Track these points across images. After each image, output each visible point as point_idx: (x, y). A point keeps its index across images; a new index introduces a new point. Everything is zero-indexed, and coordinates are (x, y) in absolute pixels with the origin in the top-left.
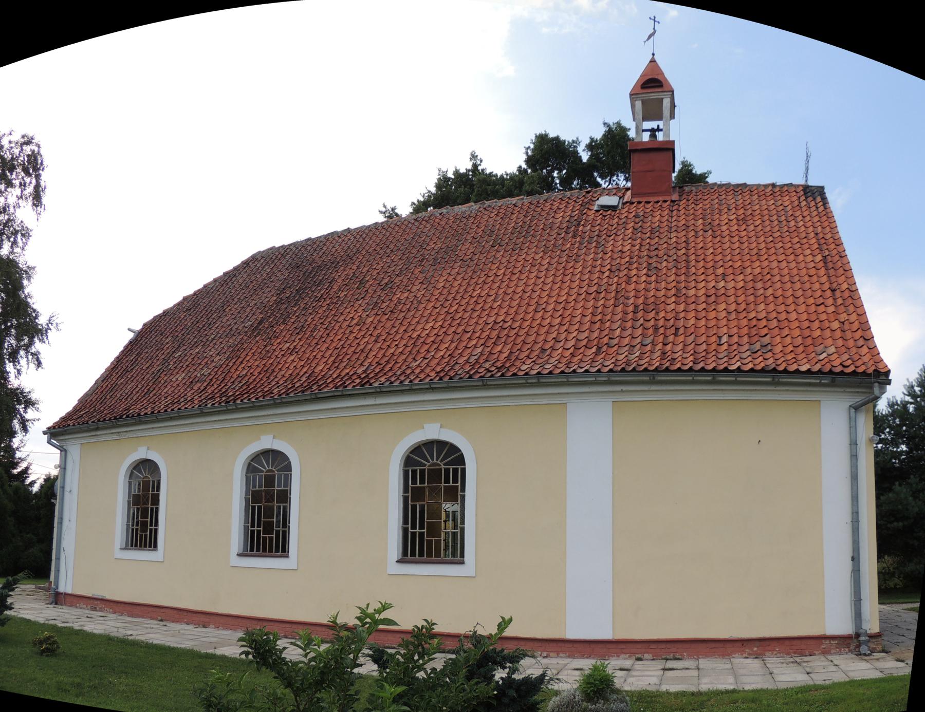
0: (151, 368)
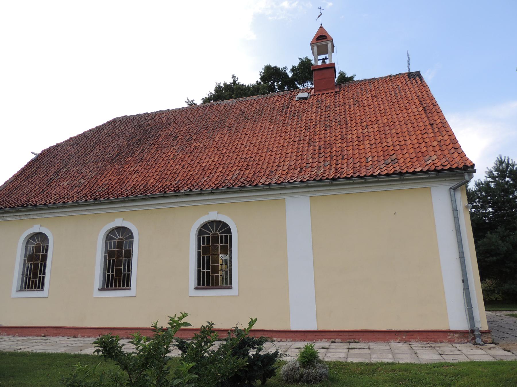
0: (45, 177)
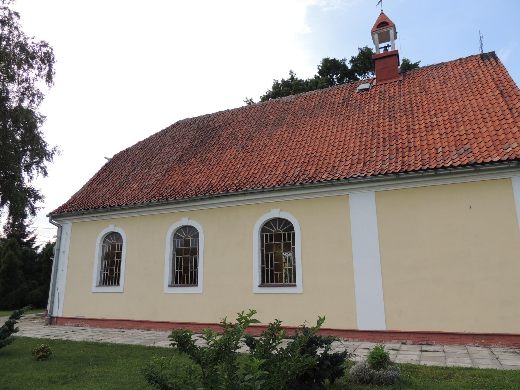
0: (118, 180)
